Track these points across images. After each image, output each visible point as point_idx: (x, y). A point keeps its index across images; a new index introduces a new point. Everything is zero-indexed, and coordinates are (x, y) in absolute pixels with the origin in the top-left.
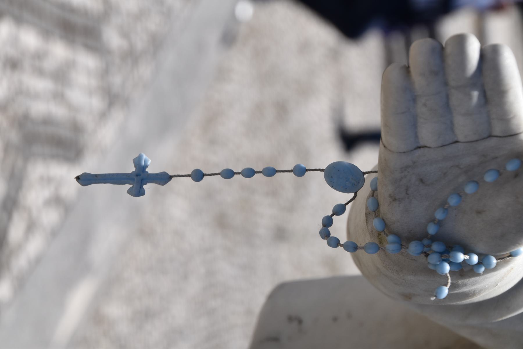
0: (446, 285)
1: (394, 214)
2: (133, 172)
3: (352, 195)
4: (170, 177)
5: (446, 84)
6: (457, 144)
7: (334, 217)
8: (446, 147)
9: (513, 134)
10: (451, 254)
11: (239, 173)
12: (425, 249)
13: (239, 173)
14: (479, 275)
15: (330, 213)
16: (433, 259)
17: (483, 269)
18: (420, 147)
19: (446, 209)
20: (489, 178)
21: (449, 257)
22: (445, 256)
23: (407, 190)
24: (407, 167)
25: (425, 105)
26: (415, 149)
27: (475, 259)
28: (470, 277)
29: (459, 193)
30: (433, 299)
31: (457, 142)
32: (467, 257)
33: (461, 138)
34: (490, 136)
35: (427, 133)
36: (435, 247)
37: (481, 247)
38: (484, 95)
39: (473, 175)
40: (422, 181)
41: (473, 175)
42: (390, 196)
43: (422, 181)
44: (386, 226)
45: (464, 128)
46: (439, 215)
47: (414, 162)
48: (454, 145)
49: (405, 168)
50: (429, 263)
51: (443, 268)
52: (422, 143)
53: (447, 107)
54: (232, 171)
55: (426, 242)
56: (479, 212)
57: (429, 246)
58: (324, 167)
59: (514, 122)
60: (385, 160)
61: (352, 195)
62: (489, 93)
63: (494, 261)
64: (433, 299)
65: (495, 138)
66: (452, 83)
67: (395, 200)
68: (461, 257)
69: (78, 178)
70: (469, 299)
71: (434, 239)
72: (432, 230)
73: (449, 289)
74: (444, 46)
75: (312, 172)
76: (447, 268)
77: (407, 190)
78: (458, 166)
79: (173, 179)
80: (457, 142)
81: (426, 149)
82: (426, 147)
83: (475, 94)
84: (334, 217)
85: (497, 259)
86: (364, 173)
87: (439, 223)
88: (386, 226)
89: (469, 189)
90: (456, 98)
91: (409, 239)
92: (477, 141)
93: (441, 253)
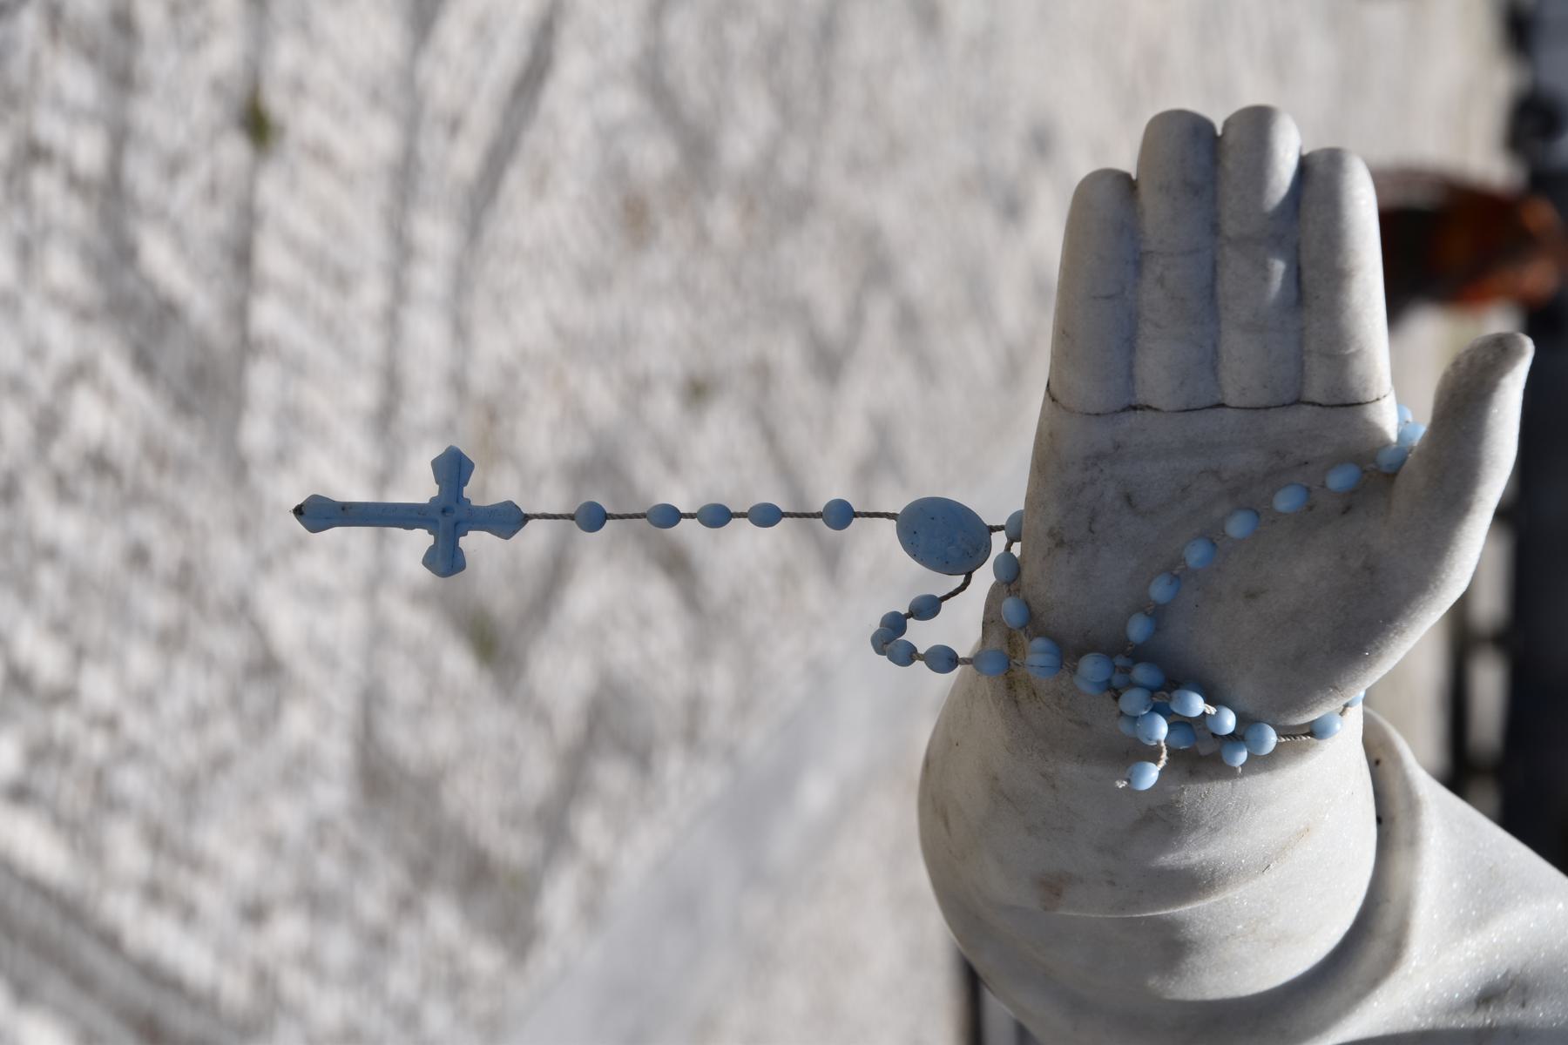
0: (1156, 761)
1: (1054, 587)
2: (433, 500)
3: (960, 579)
4: (527, 518)
5: (1215, 228)
6: (1219, 412)
7: (911, 622)
8: (1193, 414)
9: (1349, 401)
10: (1176, 694)
11: (691, 516)
12: (1117, 680)
13: (691, 516)
14: (1229, 773)
15: (904, 610)
16: (1133, 701)
17: (1242, 757)
18: (1135, 408)
19: (1177, 577)
20: (1285, 501)
21: (1170, 699)
22: (1161, 700)
23: (1092, 520)
24: (1099, 457)
25: (1161, 281)
26: (1124, 410)
27: (1229, 721)
28: (1211, 779)
29: (1213, 537)
30: (1121, 785)
31: (1222, 405)
32: (1211, 710)
33: (1231, 396)
34: (1298, 402)
35: (1157, 371)
36: (1141, 673)
37: (1247, 690)
38: (1296, 274)
39: (1246, 493)
40: (1128, 499)
41: (1246, 493)
42: (1051, 534)
43: (1128, 499)
44: (1032, 622)
45: (1243, 368)
46: (1159, 591)
47: (1118, 446)
48: (1213, 412)
49: (1096, 459)
50: (1122, 713)
51: (1152, 727)
52: (1140, 398)
53: (1211, 293)
54: (676, 510)
55: (1120, 661)
56: (1251, 595)
57: (1127, 670)
58: (898, 509)
59: (1358, 367)
60: (1051, 435)
61: (960, 579)
62: (1308, 274)
63: (1272, 739)
64: (1121, 785)
65: (1309, 408)
66: (1230, 227)
67: (1060, 544)
68: (1198, 705)
69: (299, 511)
70: (1199, 898)
71: (1138, 654)
72: (1138, 630)
73: (1162, 772)
74: (1219, 132)
75: (867, 519)
76: (1162, 729)
77: (1092, 520)
78: (1216, 473)
79: (531, 523)
80: (1222, 405)
81: (1149, 414)
82: (1149, 407)
83: (1279, 267)
84: (911, 622)
85: (1279, 736)
86: (993, 529)
87: (1157, 614)
88: (1032, 622)
89: (1238, 526)
90: (1235, 266)
91: (1080, 653)
92: (1267, 408)
93: (1153, 691)
